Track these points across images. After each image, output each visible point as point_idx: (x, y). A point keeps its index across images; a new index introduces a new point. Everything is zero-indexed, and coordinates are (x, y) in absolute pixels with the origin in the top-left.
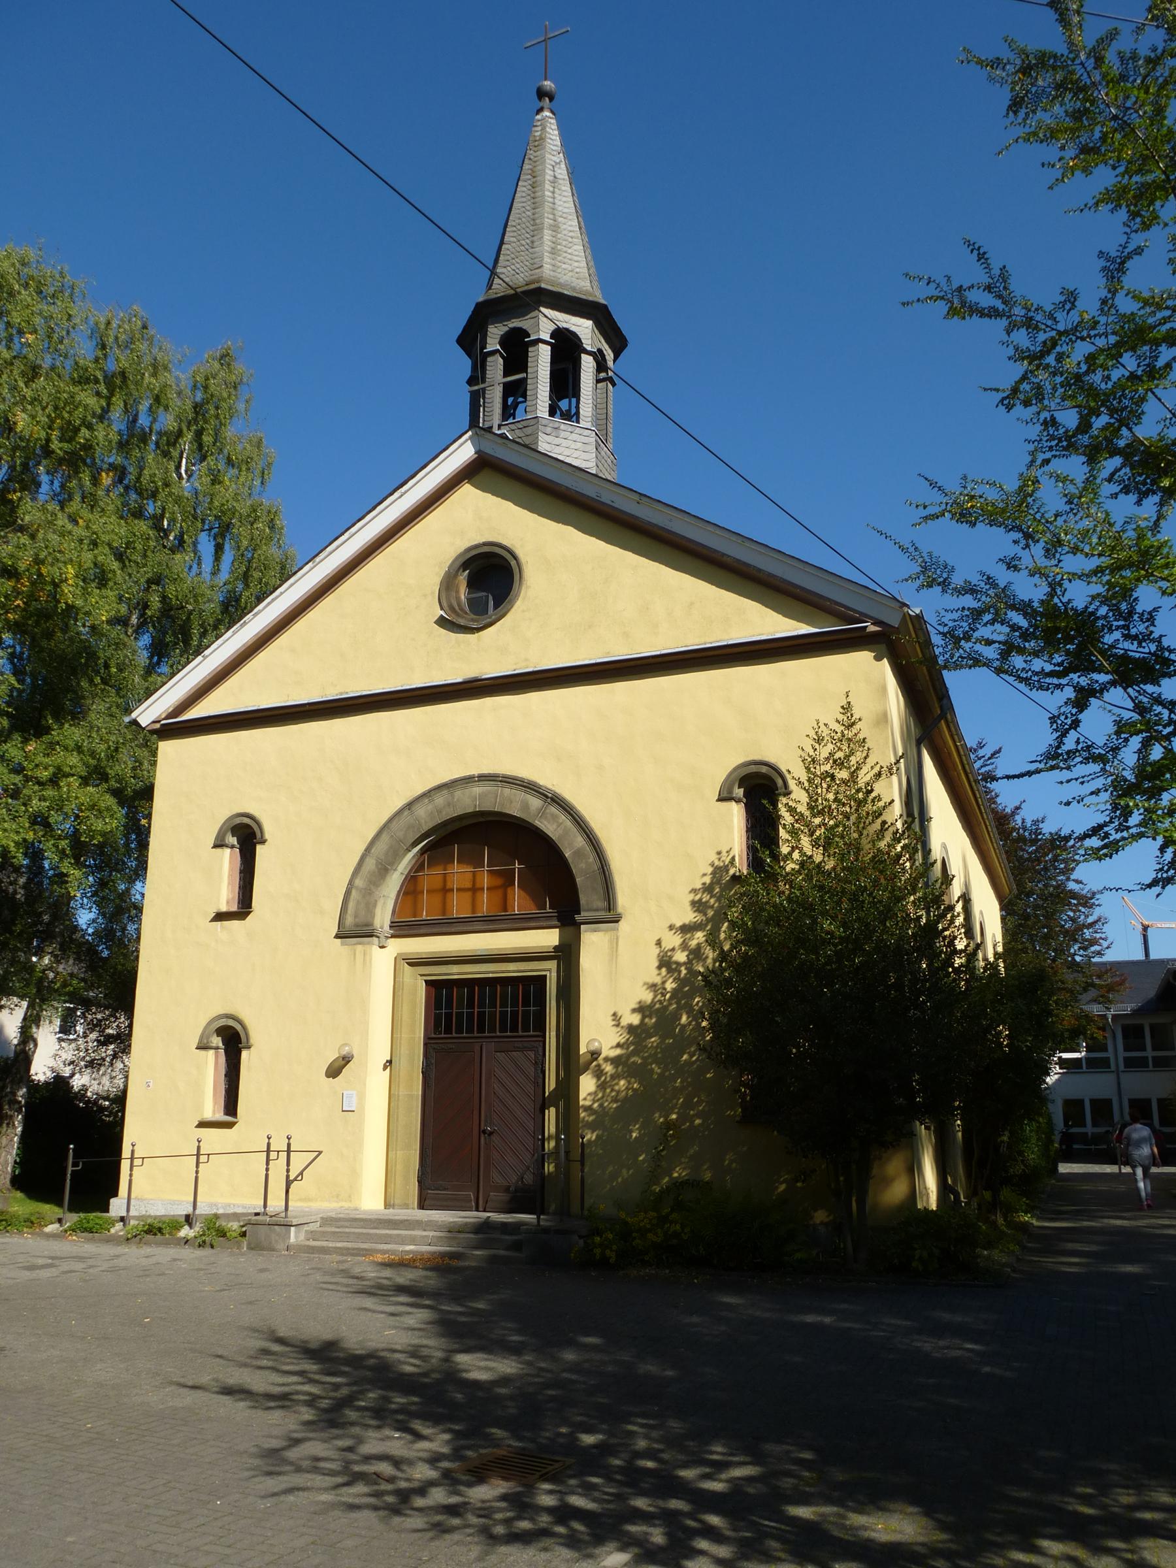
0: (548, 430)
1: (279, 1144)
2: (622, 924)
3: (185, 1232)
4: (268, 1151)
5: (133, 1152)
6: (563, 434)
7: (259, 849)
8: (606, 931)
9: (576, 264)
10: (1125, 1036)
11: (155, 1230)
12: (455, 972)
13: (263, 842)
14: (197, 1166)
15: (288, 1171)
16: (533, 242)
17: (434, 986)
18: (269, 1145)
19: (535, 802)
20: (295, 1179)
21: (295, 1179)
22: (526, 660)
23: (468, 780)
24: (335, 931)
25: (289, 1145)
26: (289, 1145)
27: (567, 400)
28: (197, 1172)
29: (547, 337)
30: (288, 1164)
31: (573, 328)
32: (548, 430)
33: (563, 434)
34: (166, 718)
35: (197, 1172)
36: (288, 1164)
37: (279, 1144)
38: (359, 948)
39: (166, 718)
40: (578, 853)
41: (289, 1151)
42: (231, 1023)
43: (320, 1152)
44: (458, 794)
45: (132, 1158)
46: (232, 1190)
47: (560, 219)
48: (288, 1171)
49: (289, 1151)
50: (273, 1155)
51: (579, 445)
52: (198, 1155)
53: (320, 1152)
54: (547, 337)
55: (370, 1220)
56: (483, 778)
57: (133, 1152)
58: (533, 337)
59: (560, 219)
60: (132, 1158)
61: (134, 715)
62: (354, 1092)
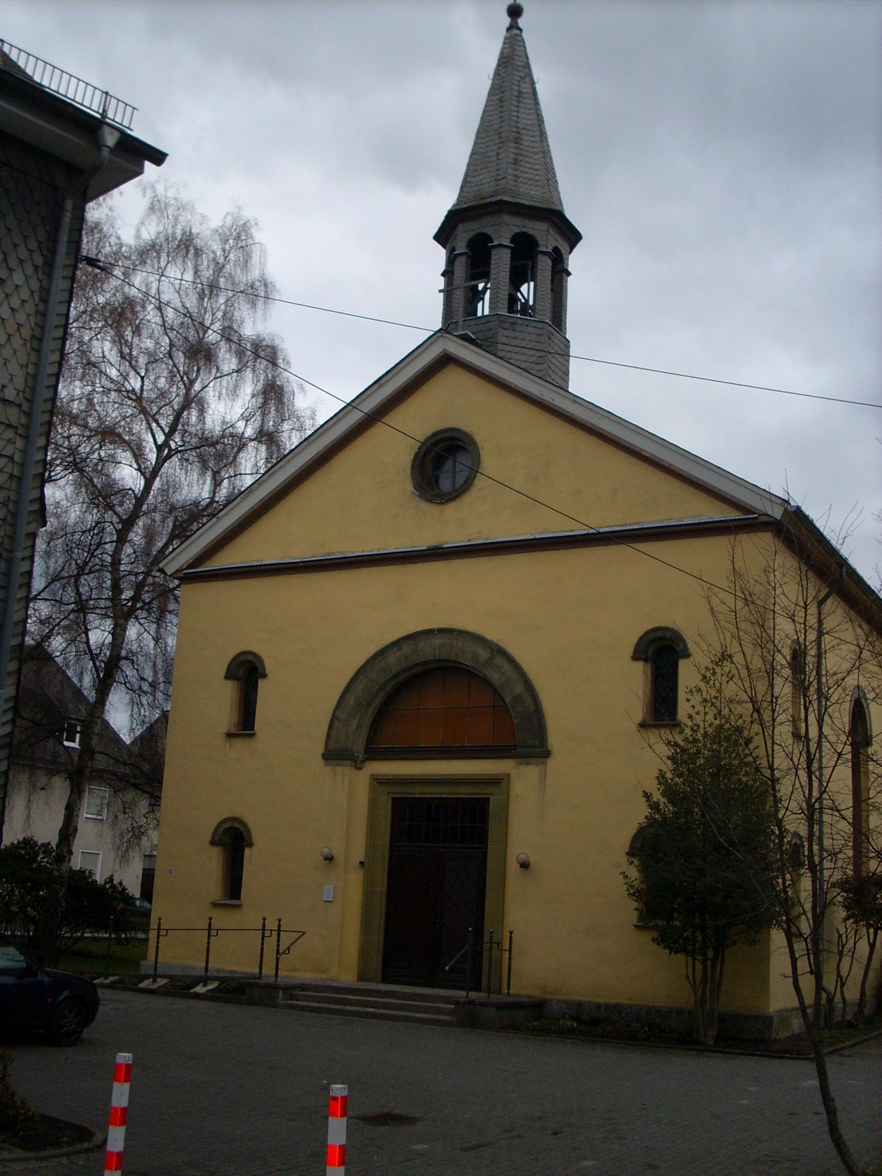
0: (507, 325)
1: (272, 925)
2: (551, 762)
3: (200, 989)
4: (264, 929)
5: (159, 924)
6: (519, 328)
7: (261, 683)
8: (537, 764)
9: (535, 173)
10: (148, 925)
11: (180, 986)
12: (417, 792)
13: (265, 676)
14: (209, 939)
15: (278, 946)
16: (498, 154)
17: (397, 802)
18: (264, 925)
19: (484, 654)
20: (284, 953)
21: (284, 953)
22: (480, 532)
23: (429, 632)
24: (320, 749)
25: (279, 925)
26: (279, 925)
27: (526, 285)
28: (208, 943)
29: (507, 242)
30: (278, 941)
31: (531, 232)
32: (507, 325)
33: (519, 328)
34: (188, 567)
35: (208, 943)
36: (278, 941)
37: (272, 925)
38: (339, 769)
39: (188, 567)
40: (517, 698)
41: (279, 931)
42: (236, 825)
43: (304, 933)
44: (422, 644)
45: (159, 930)
46: (236, 956)
47: (523, 132)
48: (278, 946)
49: (279, 931)
50: (267, 933)
51: (533, 337)
52: (210, 929)
53: (304, 933)
54: (507, 242)
55: (375, 718)
56: (441, 631)
57: (159, 924)
58: (496, 243)
59: (523, 132)
60: (159, 930)
61: (161, 565)
62: (332, 887)
